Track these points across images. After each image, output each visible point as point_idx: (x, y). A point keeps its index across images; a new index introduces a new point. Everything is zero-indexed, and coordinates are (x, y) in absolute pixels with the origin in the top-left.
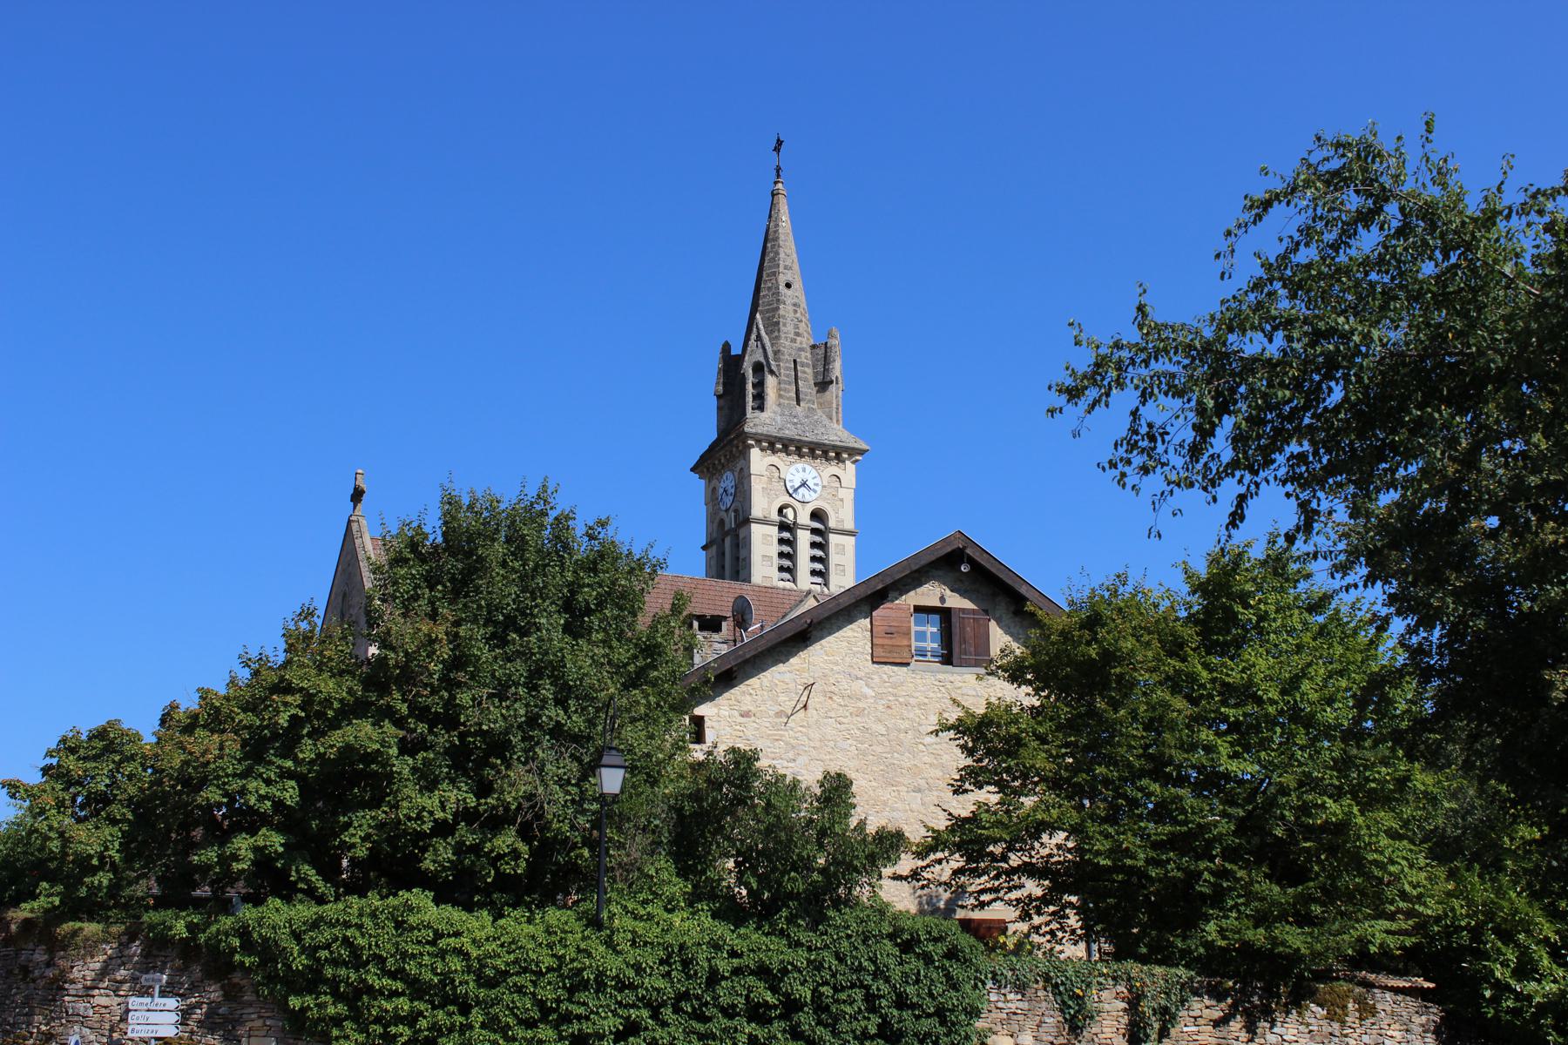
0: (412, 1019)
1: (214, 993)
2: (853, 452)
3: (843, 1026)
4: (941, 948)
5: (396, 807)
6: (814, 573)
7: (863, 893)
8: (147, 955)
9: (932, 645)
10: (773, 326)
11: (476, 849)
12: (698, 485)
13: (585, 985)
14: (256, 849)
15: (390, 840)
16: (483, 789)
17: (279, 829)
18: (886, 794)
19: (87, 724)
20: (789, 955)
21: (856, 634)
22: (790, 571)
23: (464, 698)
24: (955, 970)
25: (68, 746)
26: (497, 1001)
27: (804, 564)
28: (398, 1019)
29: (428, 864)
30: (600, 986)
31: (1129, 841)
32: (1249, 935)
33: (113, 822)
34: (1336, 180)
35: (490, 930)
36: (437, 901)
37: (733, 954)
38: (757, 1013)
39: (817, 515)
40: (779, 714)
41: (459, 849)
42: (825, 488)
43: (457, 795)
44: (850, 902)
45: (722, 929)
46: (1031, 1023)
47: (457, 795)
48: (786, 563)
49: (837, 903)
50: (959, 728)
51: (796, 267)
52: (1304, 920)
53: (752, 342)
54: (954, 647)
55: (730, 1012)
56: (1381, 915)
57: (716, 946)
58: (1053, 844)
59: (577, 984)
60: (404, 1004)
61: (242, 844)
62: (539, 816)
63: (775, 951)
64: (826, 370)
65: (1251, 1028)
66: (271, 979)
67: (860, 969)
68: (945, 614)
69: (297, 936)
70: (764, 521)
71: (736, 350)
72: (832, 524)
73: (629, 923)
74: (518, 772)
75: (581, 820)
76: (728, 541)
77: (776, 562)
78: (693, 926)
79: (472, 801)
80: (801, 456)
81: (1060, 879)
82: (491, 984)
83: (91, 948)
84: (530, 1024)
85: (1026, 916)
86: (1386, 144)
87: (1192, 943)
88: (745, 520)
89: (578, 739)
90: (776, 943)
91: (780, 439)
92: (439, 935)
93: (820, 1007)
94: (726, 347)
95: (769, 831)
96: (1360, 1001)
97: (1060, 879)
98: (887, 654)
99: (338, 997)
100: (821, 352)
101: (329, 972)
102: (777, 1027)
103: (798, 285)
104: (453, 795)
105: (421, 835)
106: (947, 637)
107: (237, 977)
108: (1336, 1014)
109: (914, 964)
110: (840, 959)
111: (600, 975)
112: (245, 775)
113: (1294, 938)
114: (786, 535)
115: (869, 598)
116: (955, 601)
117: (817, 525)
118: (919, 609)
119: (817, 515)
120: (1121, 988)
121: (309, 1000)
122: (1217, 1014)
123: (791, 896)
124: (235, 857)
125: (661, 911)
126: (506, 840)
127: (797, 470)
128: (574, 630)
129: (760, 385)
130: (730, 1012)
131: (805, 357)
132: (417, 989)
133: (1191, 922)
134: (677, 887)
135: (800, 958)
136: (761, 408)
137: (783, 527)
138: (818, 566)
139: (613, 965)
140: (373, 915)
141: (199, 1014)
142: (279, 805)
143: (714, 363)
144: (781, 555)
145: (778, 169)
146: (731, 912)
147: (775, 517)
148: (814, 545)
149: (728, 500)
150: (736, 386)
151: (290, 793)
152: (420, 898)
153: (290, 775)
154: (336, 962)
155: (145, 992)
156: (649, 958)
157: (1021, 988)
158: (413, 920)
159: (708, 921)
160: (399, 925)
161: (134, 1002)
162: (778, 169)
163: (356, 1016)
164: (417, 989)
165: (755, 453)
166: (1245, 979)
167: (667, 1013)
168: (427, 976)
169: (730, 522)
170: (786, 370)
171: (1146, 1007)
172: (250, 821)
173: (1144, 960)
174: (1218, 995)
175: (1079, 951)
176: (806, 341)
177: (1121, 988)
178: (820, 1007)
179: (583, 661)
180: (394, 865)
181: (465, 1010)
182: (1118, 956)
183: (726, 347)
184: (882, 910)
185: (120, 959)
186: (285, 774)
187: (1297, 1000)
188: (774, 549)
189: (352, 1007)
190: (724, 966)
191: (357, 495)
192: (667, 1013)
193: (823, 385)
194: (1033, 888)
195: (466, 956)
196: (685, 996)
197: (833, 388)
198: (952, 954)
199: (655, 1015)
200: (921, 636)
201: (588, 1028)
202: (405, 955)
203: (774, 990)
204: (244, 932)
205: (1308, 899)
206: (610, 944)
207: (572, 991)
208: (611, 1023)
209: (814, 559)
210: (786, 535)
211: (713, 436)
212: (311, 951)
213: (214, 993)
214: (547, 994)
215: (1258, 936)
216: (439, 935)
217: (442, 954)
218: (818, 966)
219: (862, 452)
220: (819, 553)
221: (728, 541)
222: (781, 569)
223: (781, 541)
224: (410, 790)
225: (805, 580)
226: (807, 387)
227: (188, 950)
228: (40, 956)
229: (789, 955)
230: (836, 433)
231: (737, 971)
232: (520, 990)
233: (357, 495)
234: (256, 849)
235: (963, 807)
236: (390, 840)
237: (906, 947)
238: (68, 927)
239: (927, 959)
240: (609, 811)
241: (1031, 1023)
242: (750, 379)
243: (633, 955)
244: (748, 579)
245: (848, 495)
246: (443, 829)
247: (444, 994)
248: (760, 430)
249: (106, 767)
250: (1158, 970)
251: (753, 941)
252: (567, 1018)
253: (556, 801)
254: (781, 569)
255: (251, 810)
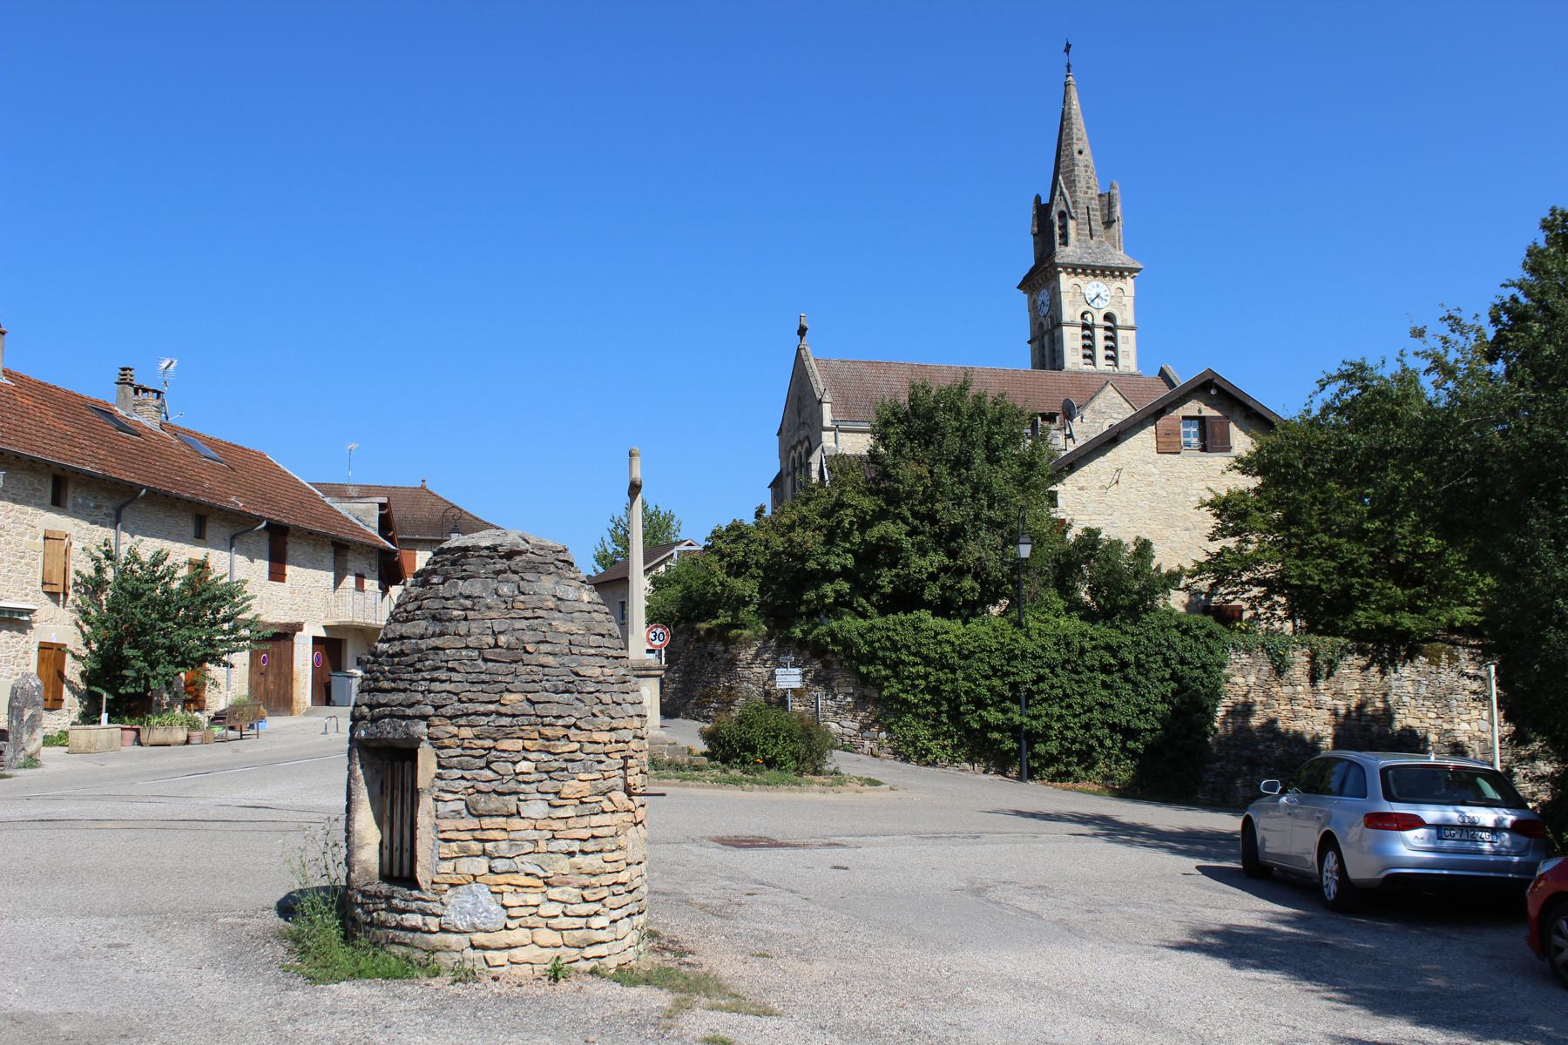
0: (926, 677)
1: (817, 665)
2: (1131, 271)
3: (1152, 675)
4: (1204, 632)
5: (906, 566)
6: (1107, 358)
7: (1160, 603)
8: (779, 646)
9: (1194, 440)
10: (1071, 183)
11: (951, 587)
12: (1023, 298)
13: (1016, 657)
14: (835, 591)
15: (906, 584)
16: (952, 554)
17: (846, 580)
18: (1168, 533)
19: (725, 523)
20: (1123, 639)
21: (1147, 436)
22: (1091, 357)
23: (938, 506)
24: (1211, 643)
25: (716, 535)
26: (970, 667)
27: (1100, 352)
28: (919, 677)
29: (927, 596)
30: (1024, 657)
31: (1309, 570)
32: (1381, 619)
33: (754, 577)
34: (1349, 377)
35: (963, 630)
36: (934, 615)
37: (1092, 639)
38: (1106, 669)
39: (1108, 317)
40: (1101, 487)
41: (943, 588)
42: (1110, 297)
43: (938, 559)
44: (1154, 609)
45: (1086, 626)
46: (1254, 671)
47: (938, 559)
48: (1088, 352)
49: (1146, 611)
50: (1212, 504)
51: (1085, 138)
52: (1414, 609)
53: (1057, 196)
54: (1210, 439)
55: (1091, 669)
56: (1464, 603)
57: (1083, 635)
58: (1267, 571)
59: (1011, 657)
60: (921, 669)
61: (828, 588)
62: (984, 569)
63: (1114, 637)
64: (1110, 213)
65: (1383, 672)
66: (849, 657)
67: (1160, 645)
68: (1202, 421)
69: (861, 635)
70: (1071, 324)
71: (1045, 200)
72: (1119, 323)
73: (1037, 625)
74: (971, 546)
75: (1005, 569)
76: (1046, 338)
77: (1081, 352)
78: (1071, 625)
79: (946, 561)
80: (1095, 276)
81: (1271, 587)
82: (967, 657)
83: (748, 643)
84: (987, 678)
85: (1253, 607)
86: (1370, 363)
87: (1349, 623)
88: (1058, 324)
89: (1000, 525)
90: (1115, 633)
91: (1080, 266)
92: (937, 634)
93: (1139, 665)
94: (1038, 199)
95: (1109, 573)
96: (1449, 653)
97: (1271, 587)
98: (1167, 446)
99: (886, 667)
100: (1106, 199)
101: (880, 654)
102: (1117, 676)
103: (1087, 151)
104: (937, 558)
105: (921, 580)
106: (1203, 435)
107: (828, 657)
108: (1434, 661)
109: (1189, 641)
110: (1150, 640)
111: (1024, 652)
112: (827, 553)
113: (1407, 621)
114: (1087, 332)
115: (1153, 415)
116: (1208, 412)
117: (1108, 324)
118: (1184, 418)
119: (1108, 317)
120: (1306, 650)
121: (871, 668)
122: (1363, 663)
123: (1122, 607)
124: (825, 596)
125: (1051, 617)
126: (968, 583)
127: (1092, 286)
128: (992, 460)
129: (1064, 227)
130: (1091, 669)
131: (1095, 204)
132: (927, 661)
133: (1349, 609)
134: (1060, 604)
135: (1128, 640)
136: (1066, 244)
137: (1085, 327)
138: (1111, 353)
139: (1030, 647)
140: (902, 623)
141: (810, 676)
142: (844, 567)
143: (1030, 211)
144: (1084, 347)
145: (1068, 66)
146: (1089, 616)
147: (1079, 320)
148: (1107, 338)
149: (1045, 309)
150: (1047, 227)
151: (850, 561)
152: (925, 614)
153: (849, 551)
154: (884, 649)
155: (780, 666)
156: (1049, 643)
157: (1248, 651)
158: (923, 626)
159: (1078, 622)
160: (916, 629)
161: (778, 671)
162: (1068, 66)
163: (896, 675)
164: (927, 661)
165: (1063, 277)
166: (1379, 643)
167: (1059, 670)
168: (933, 654)
169: (1047, 324)
170: (1081, 213)
171: (1320, 660)
172: (830, 577)
173: (1320, 633)
174: (1362, 652)
175: (1289, 625)
176: (1094, 192)
177: (1306, 650)
178: (1139, 665)
179: (1000, 479)
180: (905, 599)
181: (953, 671)
182: (1311, 629)
183: (1038, 199)
184: (1171, 613)
185: (764, 649)
186: (847, 551)
187: (1411, 656)
188: (1079, 343)
189: (894, 671)
190: (1087, 645)
191: (802, 331)
192: (1059, 670)
193: (1108, 223)
194: (1256, 591)
195: (952, 644)
196: (1068, 661)
197: (1115, 225)
198: (1209, 635)
199: (1052, 671)
200: (1187, 434)
201: (1018, 679)
202: (920, 644)
203: (1114, 657)
204: (832, 634)
205: (1419, 596)
206: (1027, 636)
207: (1008, 661)
208: (1030, 676)
209: (1107, 348)
210: (1087, 332)
211: (1033, 263)
212: (871, 643)
213: (817, 665)
214: (996, 662)
215: (1387, 620)
216: (937, 634)
217: (940, 643)
218: (1137, 644)
219: (1138, 270)
220: (1110, 344)
221: (1046, 338)
222: (1085, 356)
223: (1084, 337)
224: (915, 558)
225: (1102, 364)
226: (1097, 226)
227: (802, 644)
228: (720, 647)
229: (1123, 639)
230: (1120, 258)
231: (1094, 648)
232: (981, 660)
233: (802, 331)
234: (835, 591)
235: (1215, 547)
236: (906, 584)
237: (1184, 632)
238: (734, 632)
239: (1196, 638)
240: (1019, 566)
241: (1254, 671)
242: (1057, 223)
243: (1040, 641)
244: (1061, 368)
245: (1129, 301)
246: (933, 577)
247: (942, 664)
248: (1066, 260)
249: (741, 546)
250: (1328, 639)
251: (1101, 631)
252: (1007, 674)
253: (992, 562)
254: (1085, 356)
255: (830, 571)
